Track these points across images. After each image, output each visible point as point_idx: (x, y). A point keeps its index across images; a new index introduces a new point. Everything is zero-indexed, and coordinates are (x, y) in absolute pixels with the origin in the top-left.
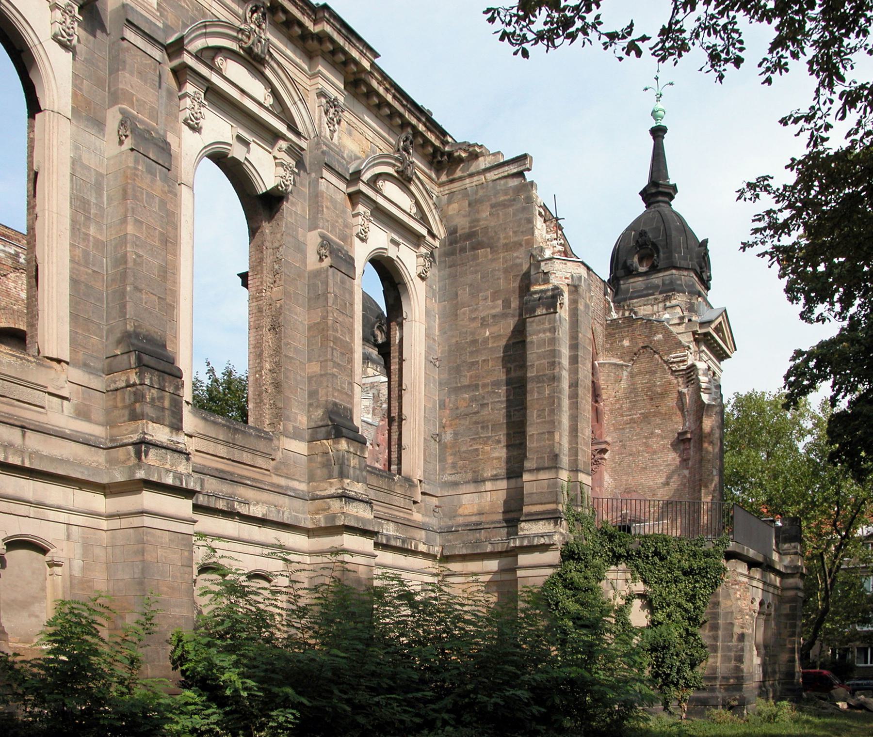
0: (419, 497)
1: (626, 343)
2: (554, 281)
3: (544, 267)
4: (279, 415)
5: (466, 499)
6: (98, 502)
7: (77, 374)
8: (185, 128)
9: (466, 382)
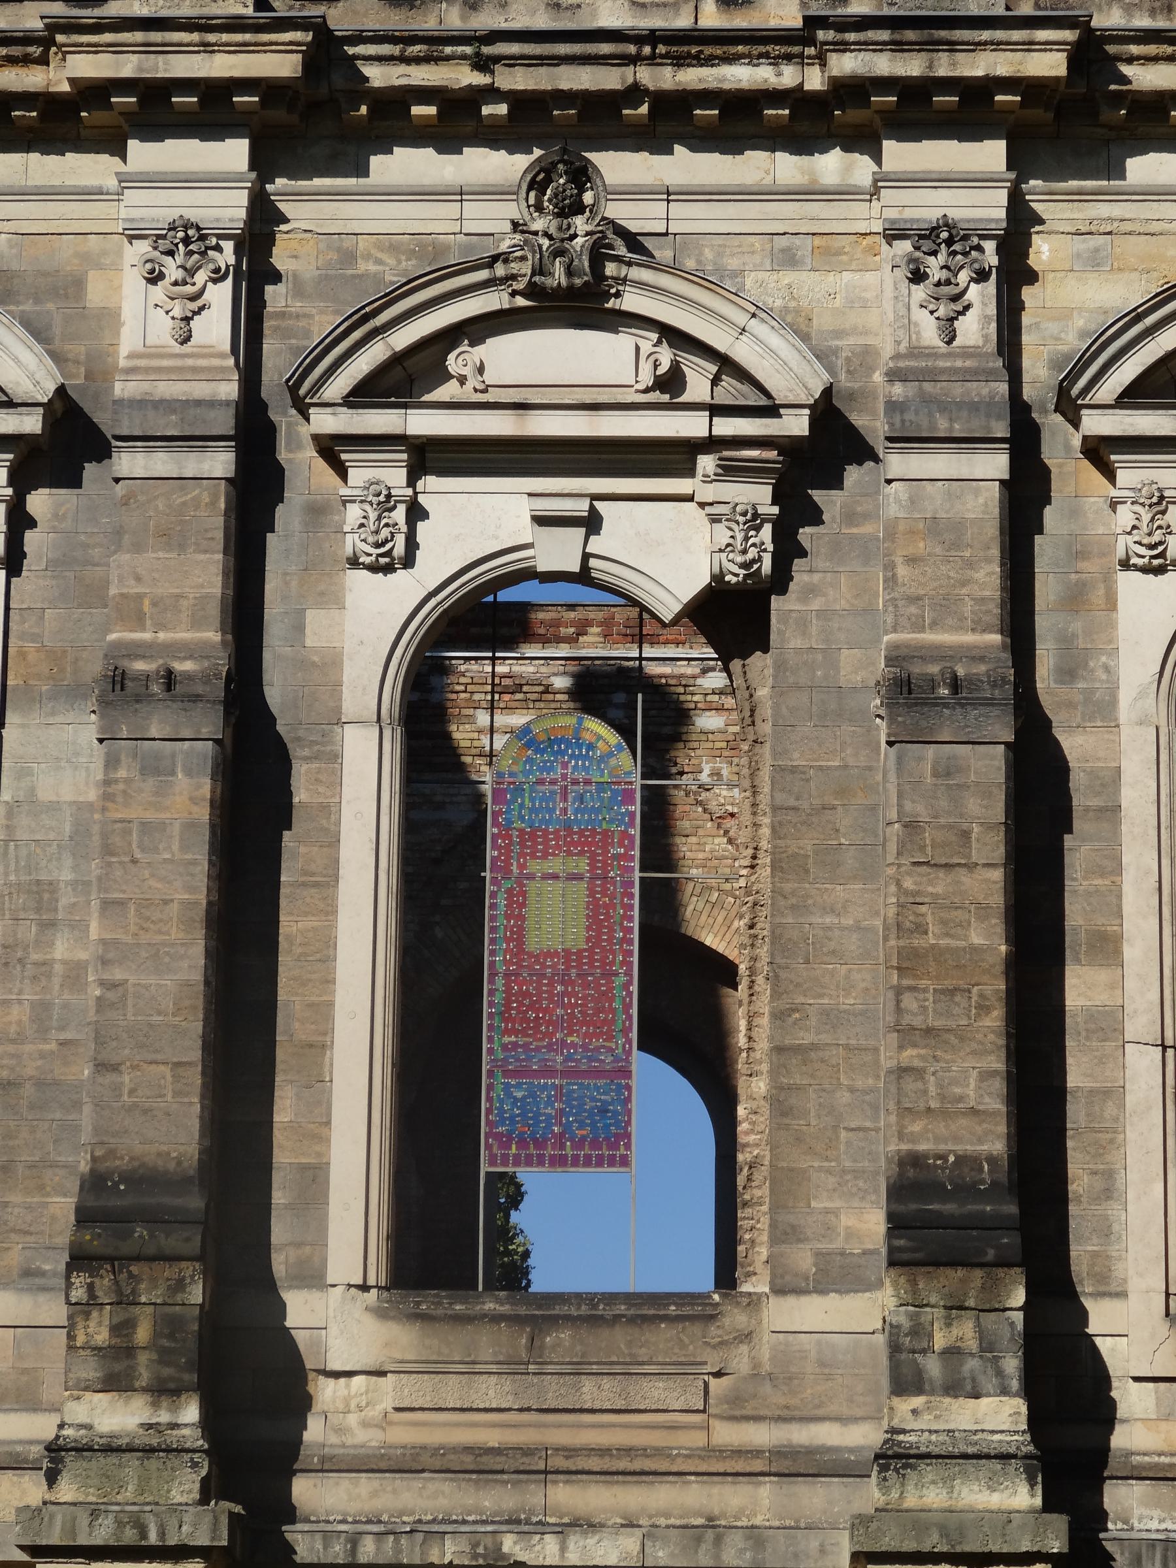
8: (955, 343)
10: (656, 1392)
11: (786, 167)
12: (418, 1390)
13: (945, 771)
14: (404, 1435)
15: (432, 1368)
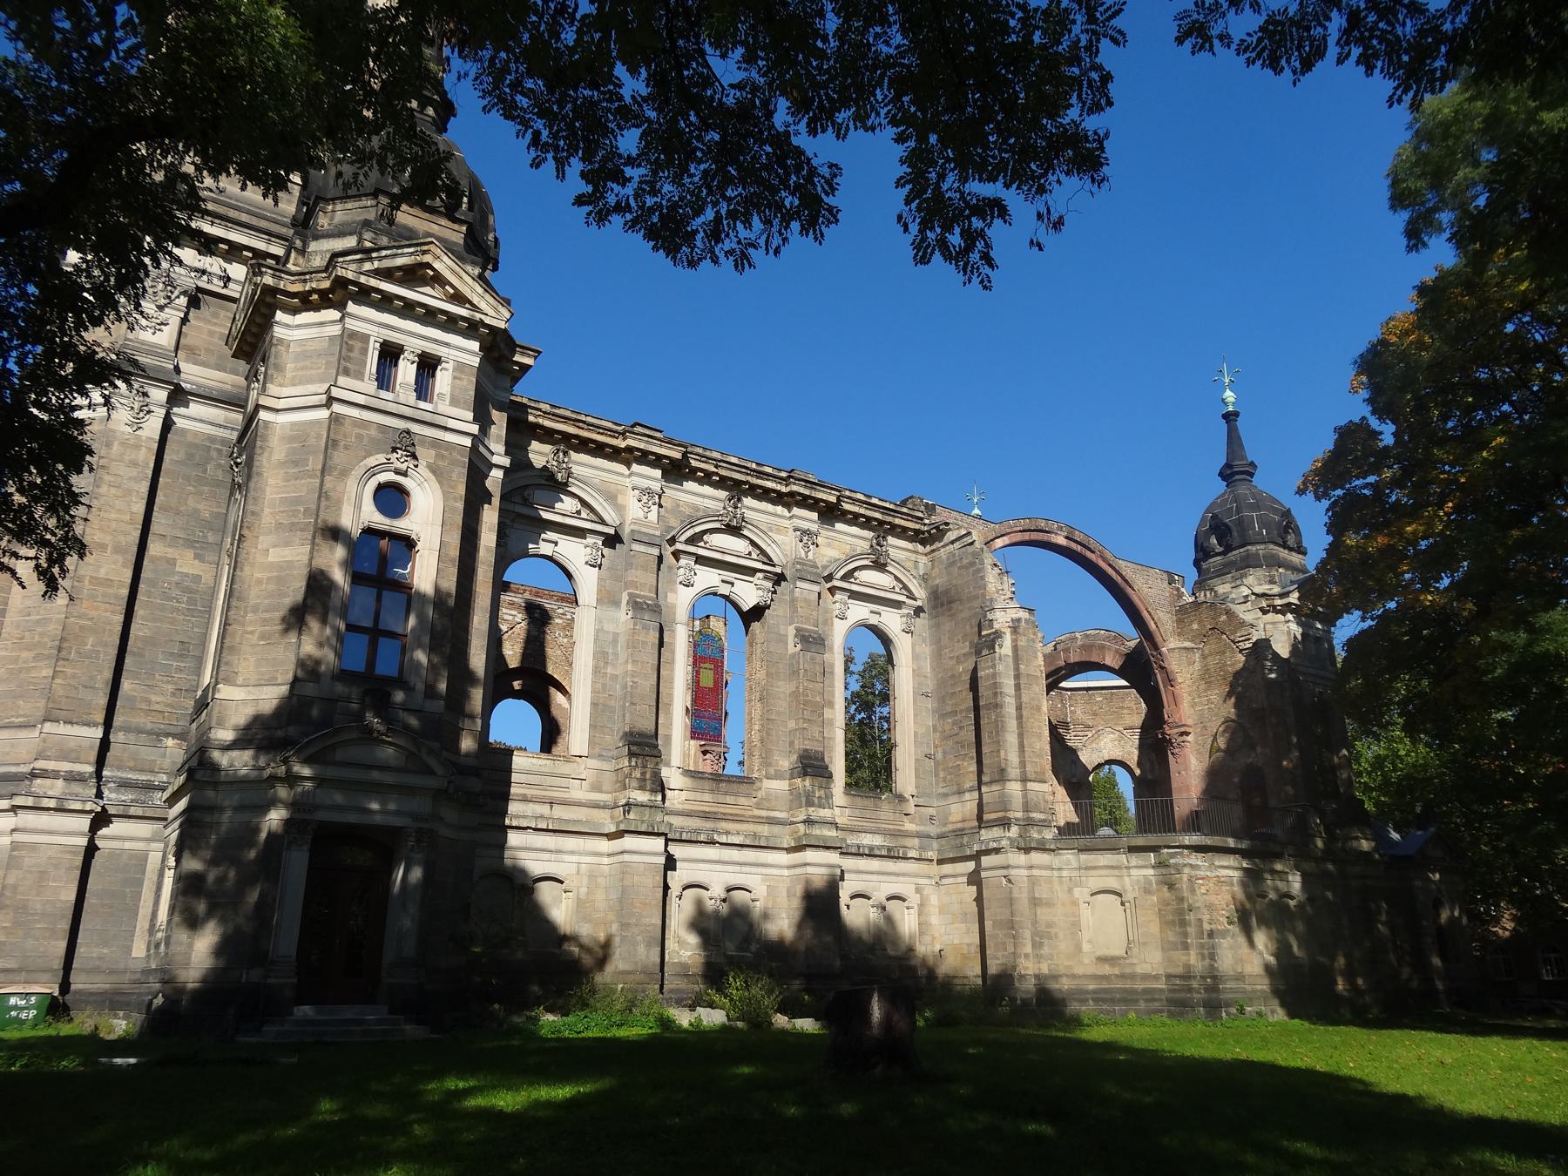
0: (912, 810)
1: (1195, 626)
2: (996, 626)
3: (989, 616)
4: (766, 762)
5: (954, 808)
6: (604, 845)
7: (593, 763)
9: (949, 709)
10: (742, 801)
11: (769, 507)
12: (691, 795)
13: (812, 659)
14: (688, 807)
15: (694, 790)
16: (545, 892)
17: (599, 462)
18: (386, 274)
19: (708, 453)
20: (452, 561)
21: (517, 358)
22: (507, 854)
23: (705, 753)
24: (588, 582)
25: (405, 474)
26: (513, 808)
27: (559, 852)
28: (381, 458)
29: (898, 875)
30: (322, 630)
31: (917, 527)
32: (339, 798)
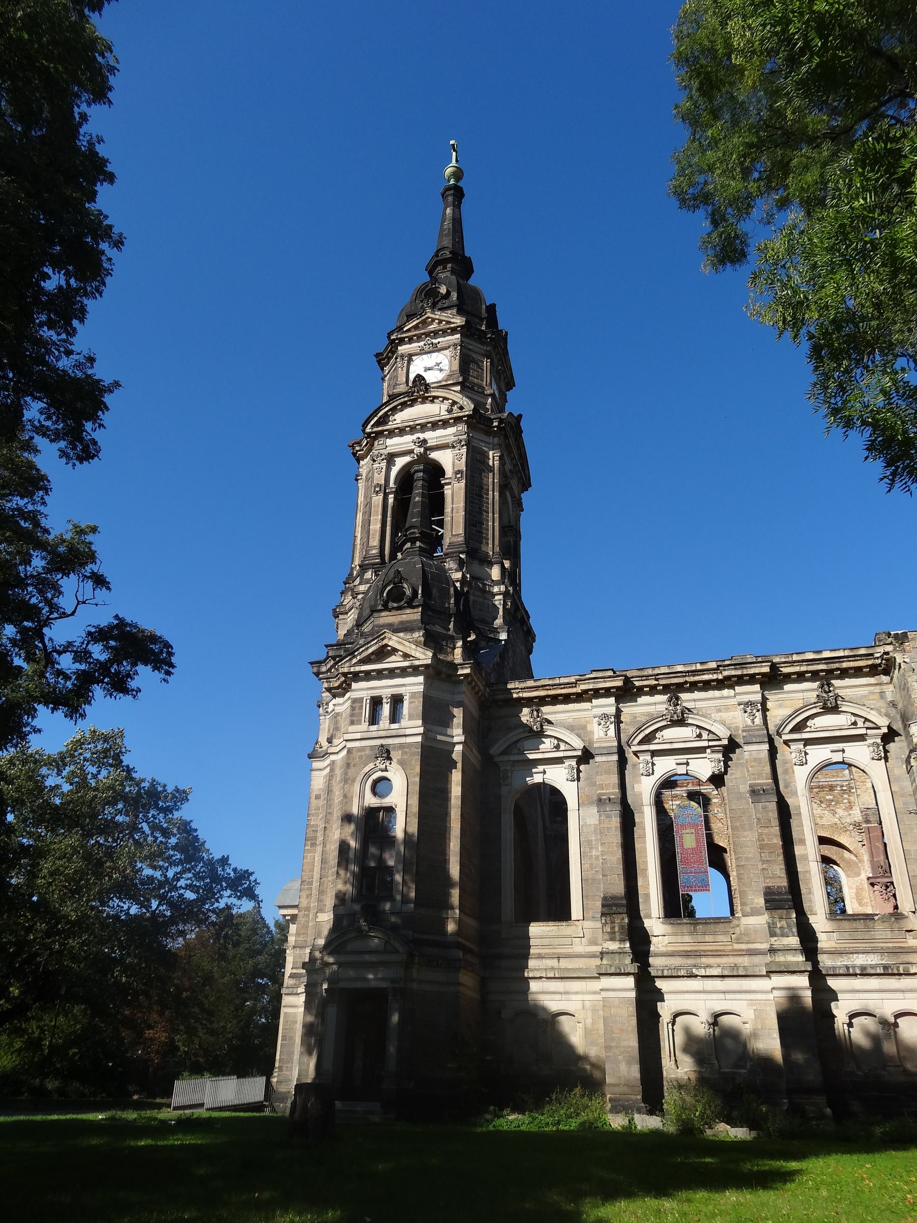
10: (721, 938)
11: (717, 693)
12: (673, 939)
14: (671, 948)
15: (674, 934)
16: (566, 1024)
17: (571, 706)
18: (363, 661)
19: (645, 673)
20: (414, 815)
21: (460, 672)
22: (530, 997)
23: (872, 885)
24: (570, 791)
25: (386, 770)
26: (532, 963)
27: (567, 993)
28: (371, 766)
29: (903, 991)
30: (346, 874)
31: (870, 662)
32: (352, 973)
